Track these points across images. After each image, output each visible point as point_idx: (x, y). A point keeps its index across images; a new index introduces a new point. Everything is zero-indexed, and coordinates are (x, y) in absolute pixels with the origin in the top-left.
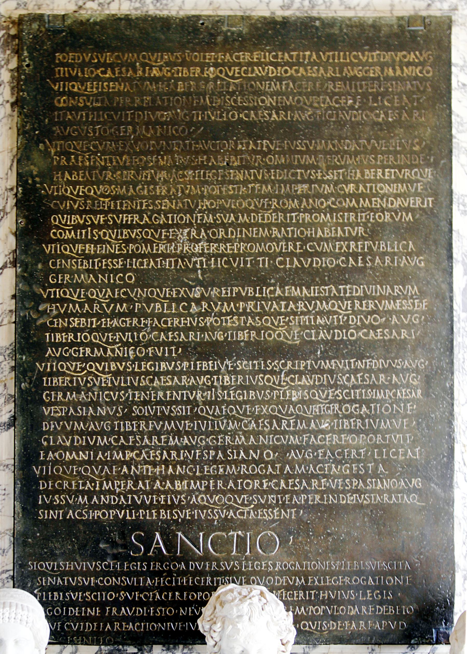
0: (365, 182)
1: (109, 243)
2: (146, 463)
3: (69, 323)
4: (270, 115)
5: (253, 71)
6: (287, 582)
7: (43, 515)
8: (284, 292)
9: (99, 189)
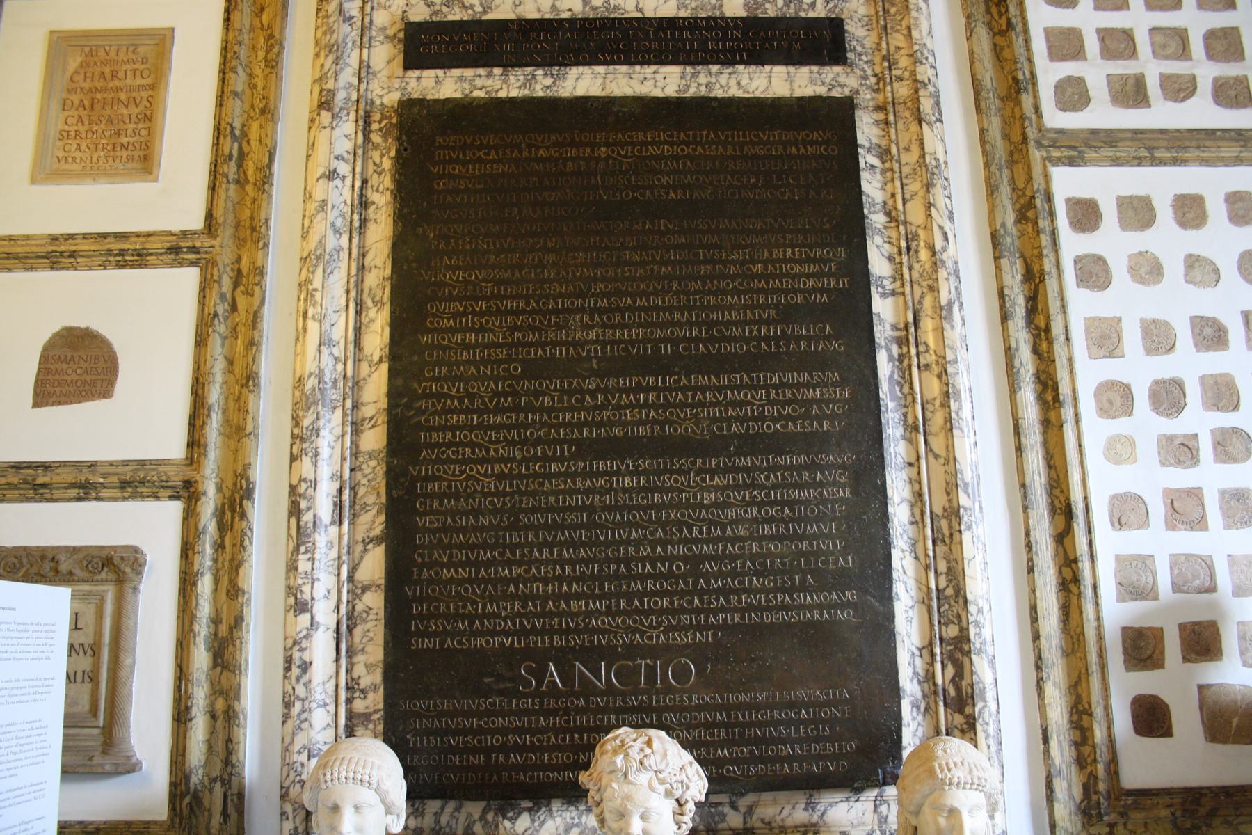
0: (773, 262)
1: (492, 331)
2: (536, 579)
3: (447, 420)
4: (667, 194)
5: (647, 150)
6: (706, 718)
7: (419, 644)
8: (690, 381)
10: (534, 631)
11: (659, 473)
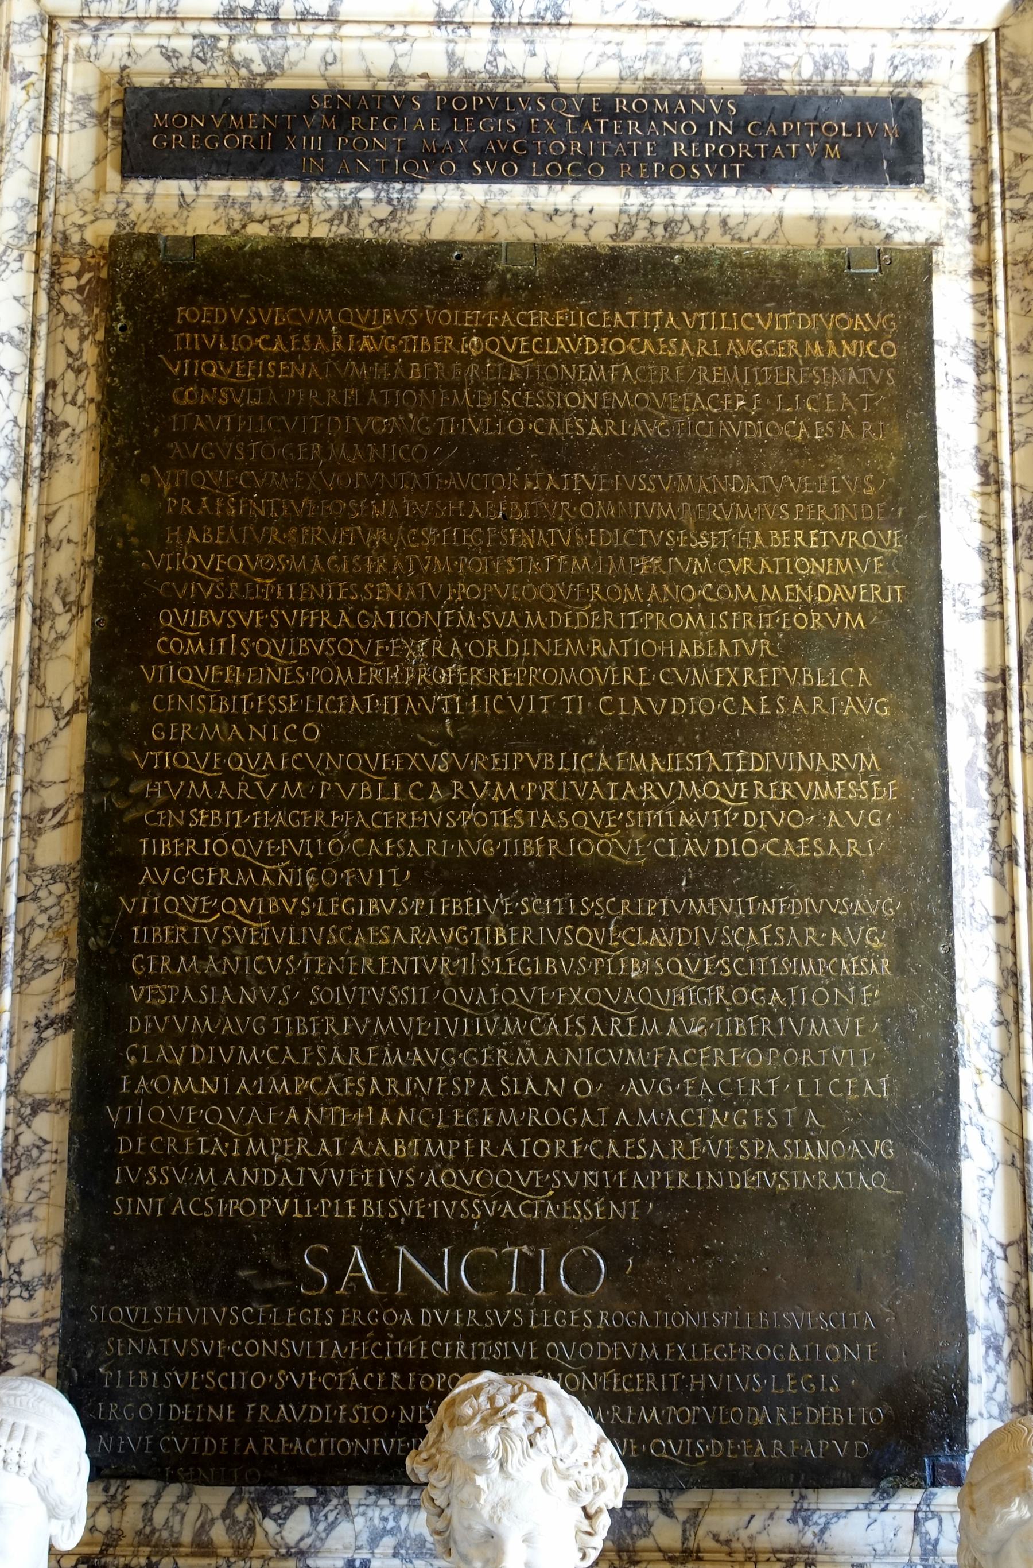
2: (335, 1101)
4: (587, 427)
6: (621, 1353)
9: (253, 561)
10: (328, 1189)
11: (555, 922)
